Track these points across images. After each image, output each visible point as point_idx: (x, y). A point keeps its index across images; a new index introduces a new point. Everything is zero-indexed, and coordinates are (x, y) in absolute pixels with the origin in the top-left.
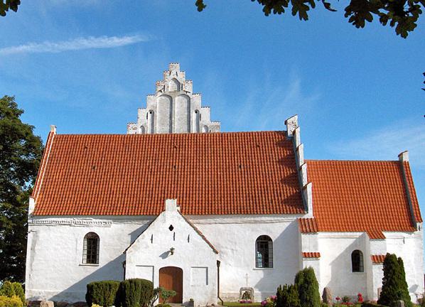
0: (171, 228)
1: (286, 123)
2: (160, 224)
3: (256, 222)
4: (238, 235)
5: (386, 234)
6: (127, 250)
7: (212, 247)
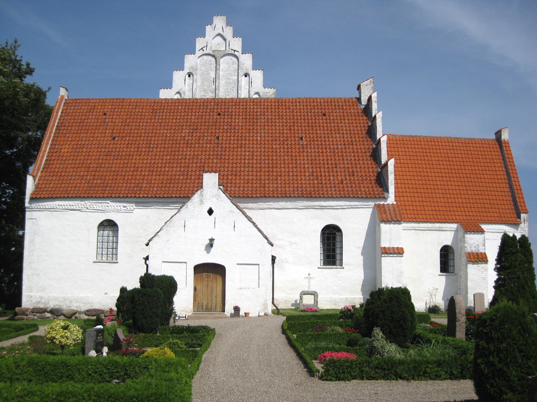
0: (210, 212)
1: (359, 88)
2: (196, 206)
3: (322, 208)
4: (298, 224)
5: (484, 227)
6: (150, 241)
7: (266, 238)
